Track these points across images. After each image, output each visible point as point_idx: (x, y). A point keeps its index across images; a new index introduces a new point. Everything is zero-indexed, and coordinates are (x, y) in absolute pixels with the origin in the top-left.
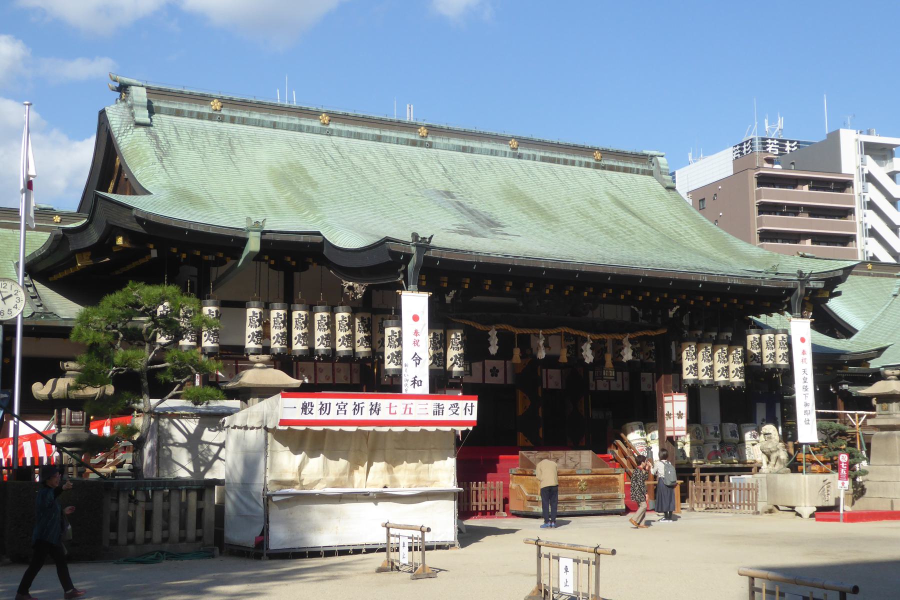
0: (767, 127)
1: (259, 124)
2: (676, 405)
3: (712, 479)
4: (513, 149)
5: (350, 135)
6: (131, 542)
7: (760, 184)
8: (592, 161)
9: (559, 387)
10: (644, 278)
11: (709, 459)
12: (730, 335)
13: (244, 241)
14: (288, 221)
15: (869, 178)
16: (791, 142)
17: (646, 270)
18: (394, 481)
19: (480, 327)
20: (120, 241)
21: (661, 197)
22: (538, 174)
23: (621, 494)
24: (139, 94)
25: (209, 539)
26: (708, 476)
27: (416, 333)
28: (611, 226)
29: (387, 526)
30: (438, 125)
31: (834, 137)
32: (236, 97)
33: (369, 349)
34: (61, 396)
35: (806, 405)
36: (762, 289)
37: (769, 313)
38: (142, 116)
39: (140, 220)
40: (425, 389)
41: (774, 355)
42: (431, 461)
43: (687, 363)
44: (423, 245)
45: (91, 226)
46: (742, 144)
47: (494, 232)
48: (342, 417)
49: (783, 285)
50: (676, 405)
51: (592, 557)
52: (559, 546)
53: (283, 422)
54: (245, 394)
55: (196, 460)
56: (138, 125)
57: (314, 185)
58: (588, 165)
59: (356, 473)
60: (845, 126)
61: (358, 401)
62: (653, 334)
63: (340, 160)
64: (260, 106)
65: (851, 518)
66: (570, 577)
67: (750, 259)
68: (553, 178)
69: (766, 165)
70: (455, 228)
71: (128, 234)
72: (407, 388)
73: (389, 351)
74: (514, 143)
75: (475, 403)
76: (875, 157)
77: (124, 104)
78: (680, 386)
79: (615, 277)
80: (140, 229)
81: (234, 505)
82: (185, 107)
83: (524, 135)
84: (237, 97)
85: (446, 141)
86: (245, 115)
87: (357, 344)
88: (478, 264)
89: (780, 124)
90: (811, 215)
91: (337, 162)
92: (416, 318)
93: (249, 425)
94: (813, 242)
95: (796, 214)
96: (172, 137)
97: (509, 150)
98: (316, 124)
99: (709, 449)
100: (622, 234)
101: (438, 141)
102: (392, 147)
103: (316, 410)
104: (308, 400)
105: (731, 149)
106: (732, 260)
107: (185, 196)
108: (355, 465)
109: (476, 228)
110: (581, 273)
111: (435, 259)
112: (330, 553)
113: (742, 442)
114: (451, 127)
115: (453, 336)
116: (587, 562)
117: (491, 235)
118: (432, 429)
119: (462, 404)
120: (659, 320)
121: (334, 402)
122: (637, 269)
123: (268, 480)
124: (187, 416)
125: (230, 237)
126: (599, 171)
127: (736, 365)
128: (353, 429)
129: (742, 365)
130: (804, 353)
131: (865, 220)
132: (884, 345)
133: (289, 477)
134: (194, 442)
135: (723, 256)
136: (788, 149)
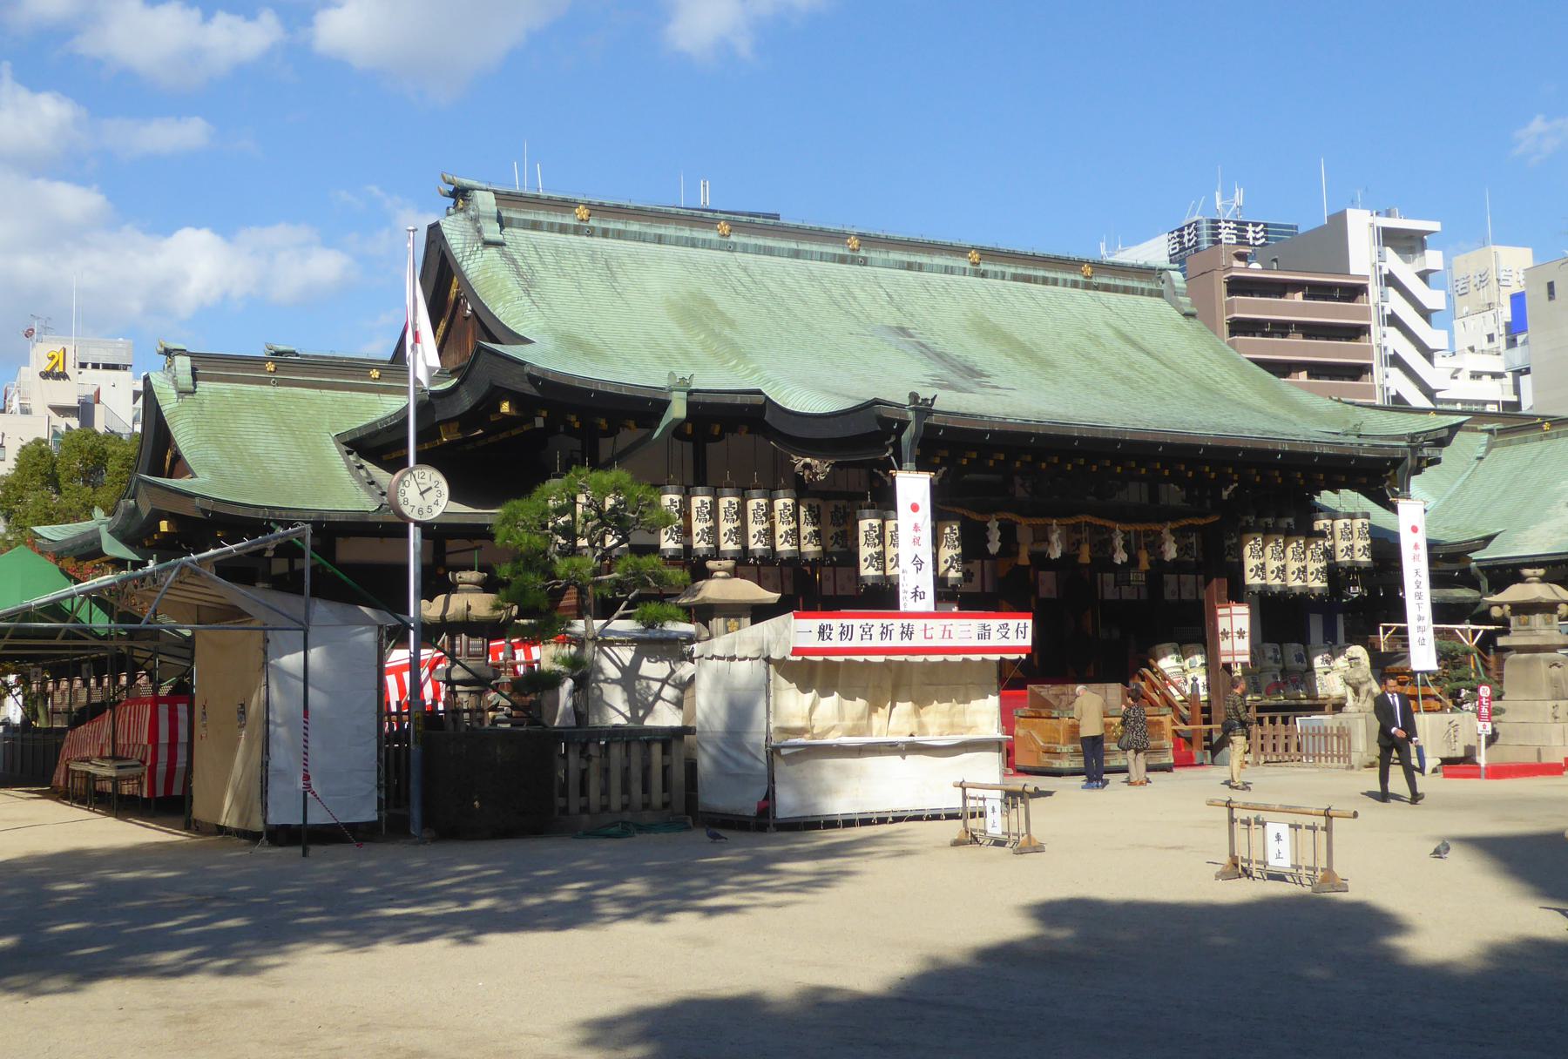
0: (1218, 203)
1: (640, 237)
2: (1235, 626)
3: (1273, 721)
4: (974, 264)
5: (759, 250)
6: (585, 809)
7: (1231, 292)
8: (1079, 278)
9: (1054, 596)
10: (1207, 448)
11: (1268, 693)
12: (1291, 520)
13: (664, 405)
14: (720, 377)
15: (1391, 280)
16: (1256, 225)
17: (1207, 437)
18: (922, 727)
19: (976, 517)
20: (505, 407)
21: (1179, 328)
22: (1011, 299)
23: (1168, 743)
24: (485, 202)
25: (679, 806)
26: (1266, 716)
27: (916, 528)
28: (1125, 371)
29: (962, 786)
30: (872, 233)
31: (1338, 223)
32: (608, 202)
33: (819, 548)
34: (459, 618)
35: (1420, 618)
36: (1359, 459)
37: (1334, 488)
38: (492, 231)
39: (533, 379)
40: (928, 604)
41: (1351, 548)
42: (966, 701)
43: (1250, 563)
44: (923, 408)
45: (462, 388)
46: (1182, 229)
47: (979, 384)
48: (867, 644)
49: (1387, 453)
50: (1235, 626)
51: (1322, 821)
52: (1267, 809)
53: (796, 651)
54: (704, 613)
55: (633, 702)
56: (488, 244)
57: (731, 323)
58: (1075, 284)
59: (874, 717)
60: (1353, 204)
61: (886, 622)
62: (1202, 522)
63: (752, 286)
64: (638, 214)
65: (1496, 772)
66: (1285, 846)
67: (1314, 414)
68: (1032, 304)
69: (1237, 263)
70: (928, 380)
71: (516, 398)
72: (907, 603)
73: (865, 551)
74: (975, 256)
75: (1029, 622)
76: (1397, 250)
77: (461, 216)
78: (1237, 592)
79: (1169, 447)
80: (533, 391)
81: (715, 761)
82: (542, 217)
83: (988, 244)
84: (608, 202)
85: (884, 256)
86: (620, 226)
87: (803, 542)
88: (992, 432)
89: (1239, 198)
90: (1306, 336)
91: (749, 290)
92: (915, 508)
93: (739, 654)
94: (1310, 376)
95: (1284, 335)
96: (533, 260)
97: (968, 266)
98: (712, 236)
99: (1267, 680)
100: (1142, 383)
101: (873, 255)
102: (815, 266)
103: (896, 634)
104: (826, 622)
105: (1165, 237)
106: (1293, 417)
107: (573, 343)
108: (874, 705)
109: (954, 378)
110: (1124, 442)
111: (938, 428)
112: (849, 823)
113: (1310, 669)
114: (890, 235)
115: (948, 530)
116: (1314, 828)
117: (978, 389)
118: (977, 657)
119: (1013, 623)
120: (1208, 503)
121: (857, 623)
122: (1196, 437)
123: (772, 727)
124: (623, 643)
125: (646, 400)
126: (1091, 292)
127: (1316, 565)
128: (880, 659)
129: (1324, 564)
130: (1416, 547)
131: (1385, 342)
132: (1493, 532)
133: (798, 723)
134: (629, 677)
135: (1282, 412)
136: (1250, 235)
